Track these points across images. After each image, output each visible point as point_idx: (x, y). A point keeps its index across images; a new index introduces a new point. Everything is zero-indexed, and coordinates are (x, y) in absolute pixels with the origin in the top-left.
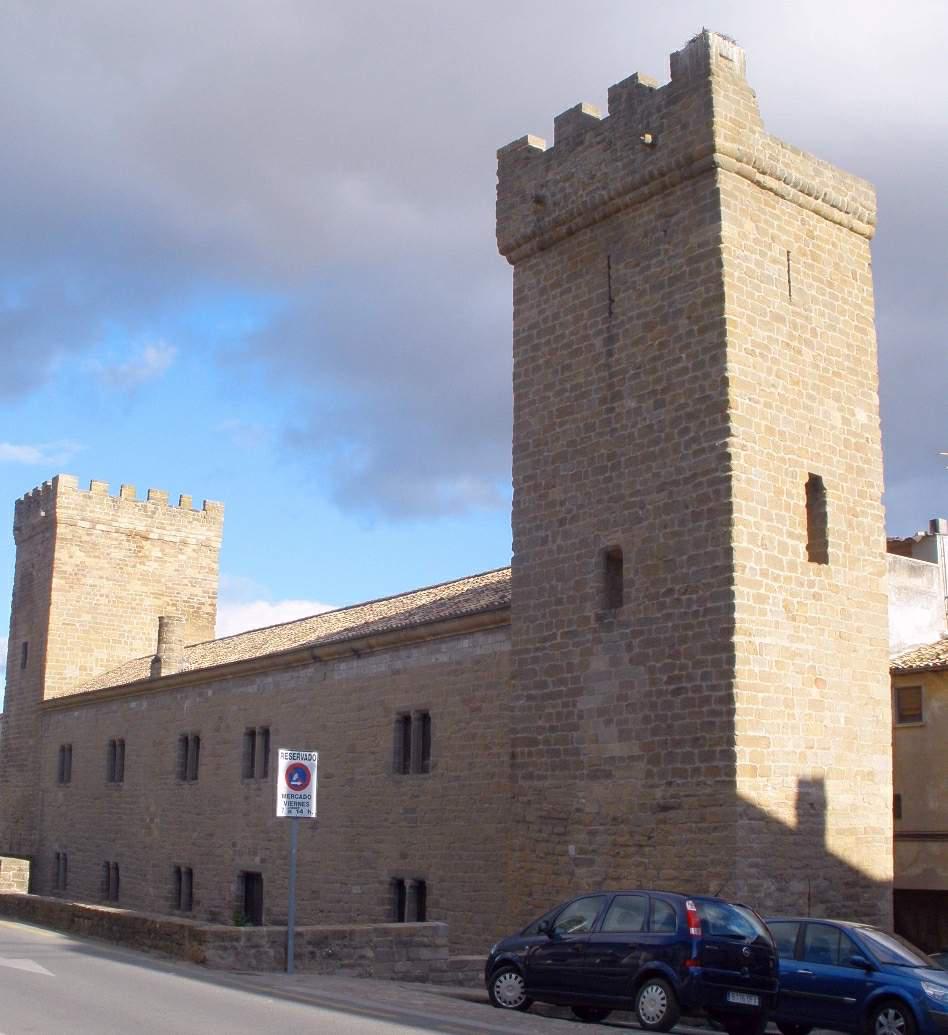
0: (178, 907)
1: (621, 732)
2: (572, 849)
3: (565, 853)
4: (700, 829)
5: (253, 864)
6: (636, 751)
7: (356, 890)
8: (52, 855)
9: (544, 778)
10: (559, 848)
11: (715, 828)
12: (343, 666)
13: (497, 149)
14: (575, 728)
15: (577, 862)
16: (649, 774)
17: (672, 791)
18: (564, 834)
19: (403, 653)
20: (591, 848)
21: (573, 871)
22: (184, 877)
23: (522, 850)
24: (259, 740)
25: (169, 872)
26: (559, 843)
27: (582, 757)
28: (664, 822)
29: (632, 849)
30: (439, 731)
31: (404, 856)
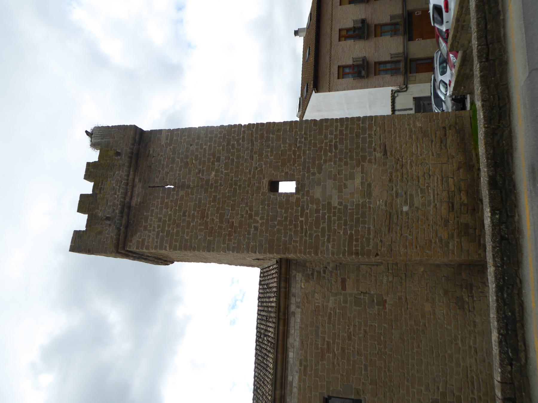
2: (405, 209)
3: (407, 213)
9: (369, 228)
21: (416, 207)
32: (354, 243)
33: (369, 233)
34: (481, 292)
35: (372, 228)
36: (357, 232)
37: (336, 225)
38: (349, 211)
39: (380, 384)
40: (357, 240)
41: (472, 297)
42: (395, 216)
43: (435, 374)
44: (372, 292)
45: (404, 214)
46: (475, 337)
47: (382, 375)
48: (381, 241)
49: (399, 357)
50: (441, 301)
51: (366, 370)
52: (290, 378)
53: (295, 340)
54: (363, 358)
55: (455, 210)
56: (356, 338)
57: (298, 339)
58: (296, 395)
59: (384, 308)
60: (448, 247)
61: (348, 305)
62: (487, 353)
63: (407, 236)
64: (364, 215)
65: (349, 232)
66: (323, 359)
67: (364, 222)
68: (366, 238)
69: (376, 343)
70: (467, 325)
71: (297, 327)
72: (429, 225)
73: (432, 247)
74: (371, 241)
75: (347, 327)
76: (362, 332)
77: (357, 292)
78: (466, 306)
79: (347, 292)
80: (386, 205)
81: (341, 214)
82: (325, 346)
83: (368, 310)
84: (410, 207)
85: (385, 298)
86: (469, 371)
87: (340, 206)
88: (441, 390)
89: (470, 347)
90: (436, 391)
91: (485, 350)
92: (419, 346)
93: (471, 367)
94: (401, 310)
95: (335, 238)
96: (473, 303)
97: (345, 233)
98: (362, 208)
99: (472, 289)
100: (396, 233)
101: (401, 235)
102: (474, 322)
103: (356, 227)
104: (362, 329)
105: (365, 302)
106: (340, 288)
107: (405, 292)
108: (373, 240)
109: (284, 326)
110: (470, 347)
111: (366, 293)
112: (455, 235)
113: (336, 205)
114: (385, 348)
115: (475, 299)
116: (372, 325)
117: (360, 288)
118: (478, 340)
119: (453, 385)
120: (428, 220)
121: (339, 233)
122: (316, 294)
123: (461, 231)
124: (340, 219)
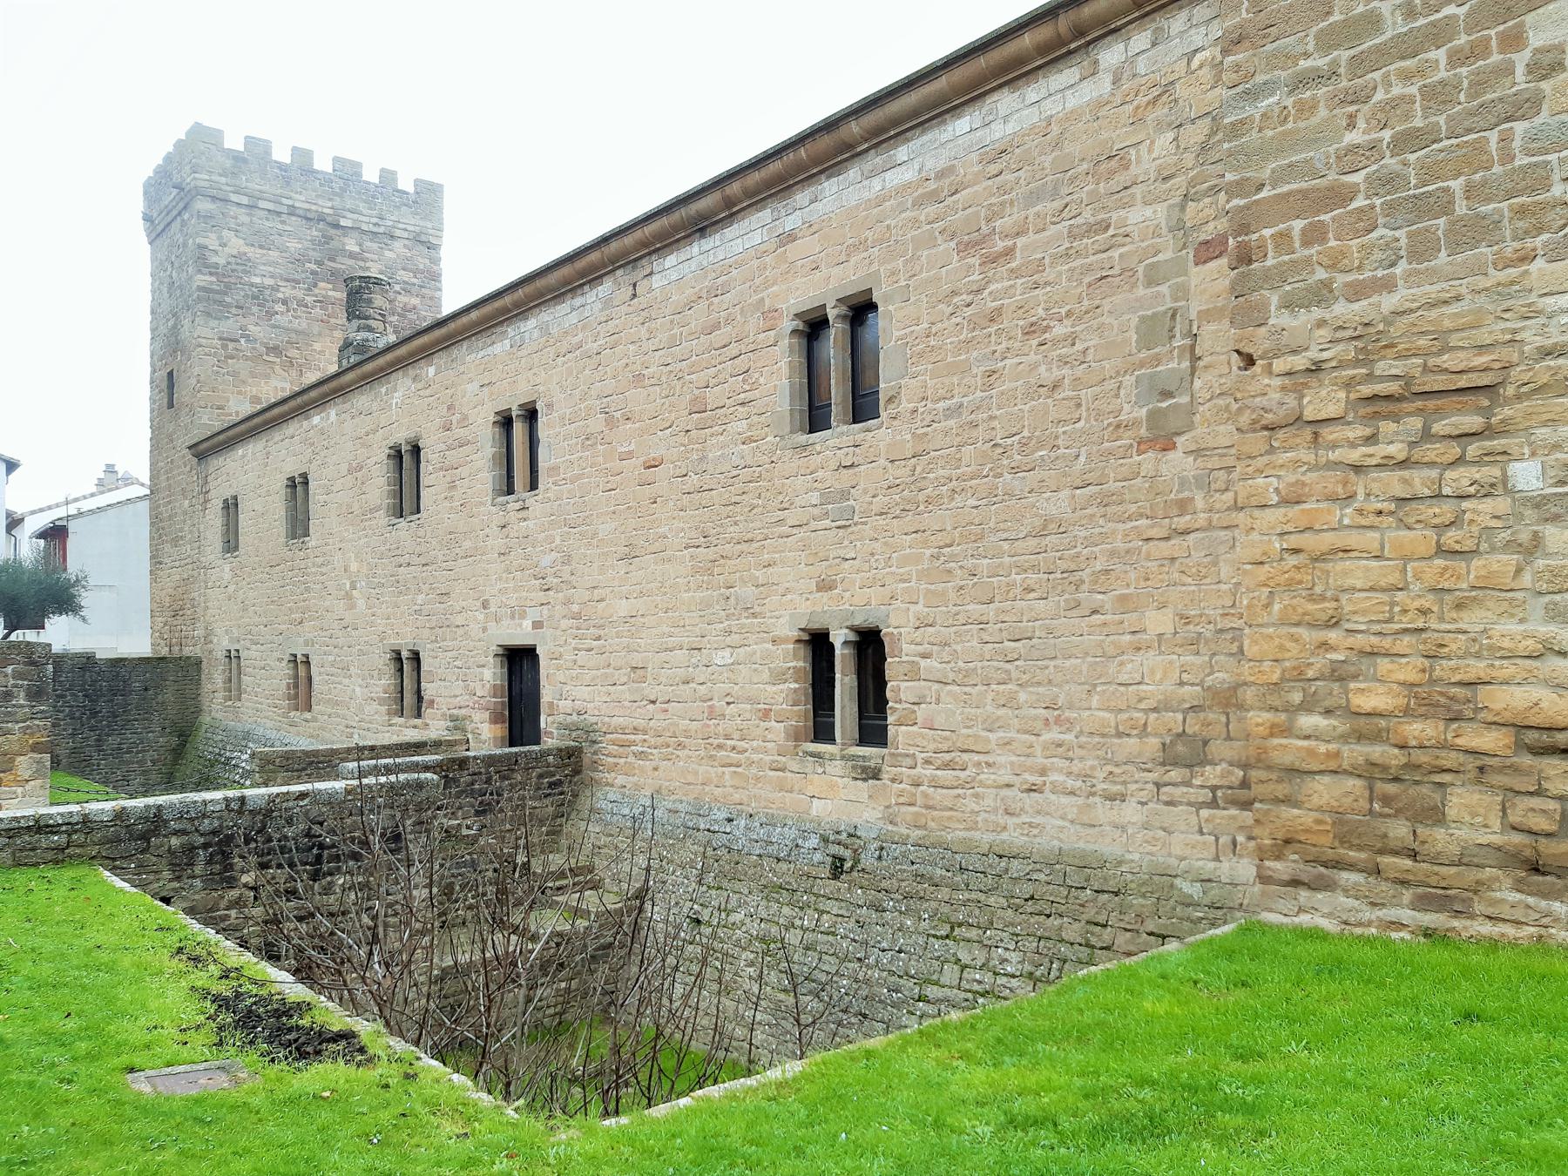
2: (1527, 475)
3: (1502, 486)
8: (220, 654)
9: (1388, 285)
12: (671, 260)
19: (801, 197)
21: (1537, 538)
22: (407, 664)
24: (519, 429)
25: (383, 661)
26: (1460, 461)
31: (825, 586)
32: (1298, 225)
33: (1356, 292)
34: (1234, 843)
35: (1389, 302)
36: (1366, 222)
37: (1396, 91)
38: (1493, 136)
39: (919, 469)
40: (1314, 235)
41: (1213, 804)
42: (1473, 422)
43: (958, 648)
44: (1198, 383)
45: (1490, 473)
46: (1072, 793)
47: (941, 472)
48: (1316, 369)
49: (992, 525)
50: (1185, 676)
51: (950, 413)
52: (902, 152)
53: (1006, 119)
54: (979, 394)
55: (1527, 760)
56: (1032, 357)
57: (1011, 128)
58: (866, 195)
59: (1142, 445)
60: (1306, 707)
61: (1141, 291)
62: (1030, 825)
63: (1351, 497)
64: (1475, 231)
65: (1357, 178)
66: (964, 248)
67: (1421, 249)
68: (1326, 285)
69: (1026, 433)
70: (1109, 768)
71: (1052, 107)
72: (1424, 612)
73: (1300, 630)
74: (1317, 313)
75: (1063, 311)
76: (1057, 373)
77: (1193, 315)
78: (1175, 774)
79: (1194, 270)
80: (1547, 353)
81: (1471, 97)
82: (1001, 245)
83: (1129, 380)
84: (1539, 503)
85: (1180, 440)
86: (976, 757)
87: (1531, 69)
88: (923, 663)
89: (1043, 772)
90: (919, 648)
91: (1038, 820)
92: (1029, 590)
93: (988, 765)
94: (1141, 515)
95: (1323, 112)
96: (1190, 804)
97: (1352, 158)
98: (1521, 212)
99: (1235, 803)
100: (1371, 439)
101: (1357, 468)
102: (1123, 798)
103: (1390, 208)
104: (1066, 371)
105: (1157, 360)
106: (1203, 237)
107: (1210, 527)
108: (1321, 323)
109: (1043, 49)
110: (1043, 772)
111: (1195, 359)
112: (1377, 752)
113: (1536, 40)
114: (1014, 470)
115: (1205, 813)
116: (1079, 405)
117: (1212, 327)
118: (1065, 800)
119: (938, 701)
120: (1459, 606)
121: (1352, 125)
122: (1170, 135)
123: (1396, 779)
124: (1437, 96)
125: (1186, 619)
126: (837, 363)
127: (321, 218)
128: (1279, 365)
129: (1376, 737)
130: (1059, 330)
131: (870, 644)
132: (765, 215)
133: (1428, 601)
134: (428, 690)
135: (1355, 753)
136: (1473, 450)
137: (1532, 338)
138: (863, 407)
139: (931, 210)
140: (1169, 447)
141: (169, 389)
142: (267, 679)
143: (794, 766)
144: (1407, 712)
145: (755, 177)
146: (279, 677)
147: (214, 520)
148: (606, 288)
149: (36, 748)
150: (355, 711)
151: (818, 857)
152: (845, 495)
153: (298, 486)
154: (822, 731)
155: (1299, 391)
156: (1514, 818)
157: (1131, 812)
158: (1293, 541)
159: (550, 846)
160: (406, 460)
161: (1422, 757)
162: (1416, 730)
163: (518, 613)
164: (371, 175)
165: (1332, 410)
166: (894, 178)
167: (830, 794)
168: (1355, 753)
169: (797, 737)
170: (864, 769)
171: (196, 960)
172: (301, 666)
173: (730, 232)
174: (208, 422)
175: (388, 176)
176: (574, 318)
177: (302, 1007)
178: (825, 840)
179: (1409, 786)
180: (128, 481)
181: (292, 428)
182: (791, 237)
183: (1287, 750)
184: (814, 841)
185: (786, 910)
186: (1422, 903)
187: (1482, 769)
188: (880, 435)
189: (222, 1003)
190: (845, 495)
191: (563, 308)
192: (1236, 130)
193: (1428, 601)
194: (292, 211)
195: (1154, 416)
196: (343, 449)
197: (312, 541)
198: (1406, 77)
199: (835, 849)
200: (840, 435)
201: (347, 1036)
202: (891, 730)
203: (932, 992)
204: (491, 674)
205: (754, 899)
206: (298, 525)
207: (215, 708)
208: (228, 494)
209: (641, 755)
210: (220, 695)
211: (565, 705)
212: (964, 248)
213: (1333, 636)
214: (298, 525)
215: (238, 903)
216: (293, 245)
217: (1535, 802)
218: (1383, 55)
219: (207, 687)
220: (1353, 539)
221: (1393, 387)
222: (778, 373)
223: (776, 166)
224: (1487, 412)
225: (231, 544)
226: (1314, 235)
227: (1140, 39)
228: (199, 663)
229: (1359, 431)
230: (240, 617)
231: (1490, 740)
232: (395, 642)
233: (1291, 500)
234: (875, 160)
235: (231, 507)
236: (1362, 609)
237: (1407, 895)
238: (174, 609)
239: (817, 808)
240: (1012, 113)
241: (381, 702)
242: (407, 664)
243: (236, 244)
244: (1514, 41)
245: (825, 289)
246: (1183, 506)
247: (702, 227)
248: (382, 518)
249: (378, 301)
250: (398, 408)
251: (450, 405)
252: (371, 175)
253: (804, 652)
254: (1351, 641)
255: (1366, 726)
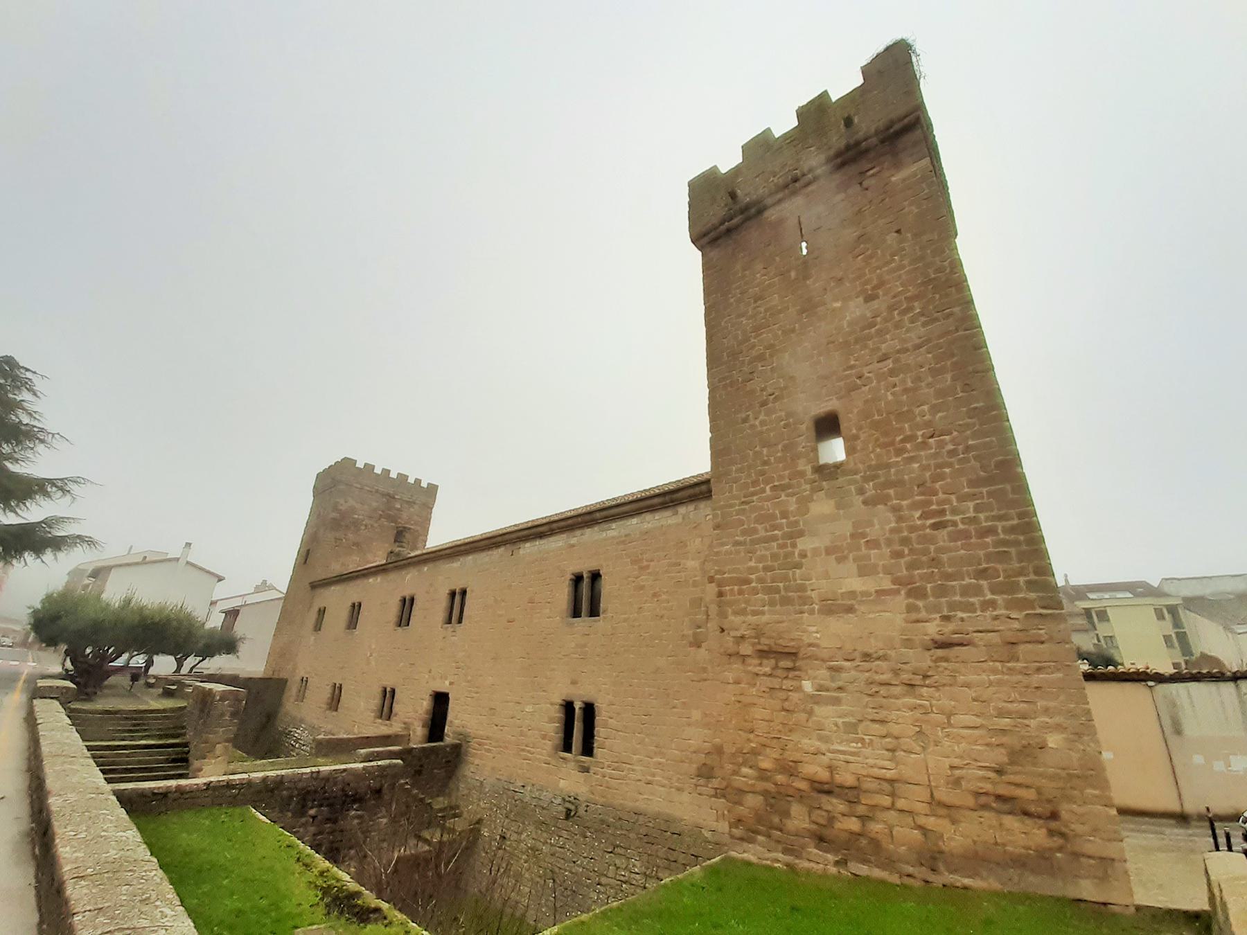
0: (381, 717)
1: (859, 568)
2: (807, 686)
3: (799, 689)
4: (1009, 669)
5: (443, 687)
6: (887, 584)
7: (529, 709)
8: (298, 678)
9: (763, 613)
10: (787, 684)
11: (1039, 670)
12: (528, 545)
13: (918, 47)
14: (798, 566)
15: (816, 700)
16: (911, 609)
17: (951, 627)
18: (793, 669)
19: (578, 533)
20: (834, 685)
21: (812, 709)
22: (388, 696)
23: (737, 682)
24: (458, 598)
25: (377, 692)
26: (786, 678)
27: (809, 593)
28: (946, 660)
29: (897, 690)
30: (607, 587)
31: (574, 683)
33: (755, 613)
36: (755, 592)
40: (741, 592)
41: (715, 796)
45: (794, 683)
48: (742, 637)
51: (625, 620)
52: (614, 525)
55: (815, 795)
59: (691, 645)
60: (744, 764)
64: (786, 601)
71: (663, 522)
78: (702, 781)
100: (760, 665)
124: (774, 557)
125: (706, 715)
126: (586, 595)
127: (388, 495)
128: (733, 633)
129: (766, 779)
130: (664, 597)
131: (589, 709)
132: (564, 536)
133: (780, 727)
134: (396, 707)
135: (762, 785)
136: (791, 674)
137: (807, 641)
138: (594, 612)
139: (622, 547)
140: (699, 647)
141: (306, 557)
142: (319, 694)
143: (553, 762)
144: (776, 770)
145: (563, 524)
146: (326, 693)
147: (313, 615)
148: (502, 550)
149: (227, 741)
150: (359, 718)
151: (560, 808)
152: (585, 646)
153: (356, 609)
154: (567, 747)
155: (738, 644)
156: (813, 818)
157: (685, 797)
158: (739, 698)
159: (441, 792)
160: (407, 604)
161: (782, 790)
162: (780, 778)
163: (443, 677)
164: (411, 480)
165: (749, 653)
166: (611, 533)
167: (568, 779)
168: (762, 785)
169: (556, 749)
170: (583, 767)
171: (306, 865)
172: (337, 692)
173: (551, 539)
174: (320, 574)
175: (418, 481)
176: (487, 559)
177: (358, 894)
178: (564, 799)
179: (777, 800)
180: (272, 588)
181: (359, 582)
182: (573, 546)
183: (739, 781)
184: (559, 801)
185: (545, 835)
186: (786, 851)
187: (801, 797)
188: (600, 623)
189: (326, 891)
190: (585, 646)
191: (483, 555)
192: (717, 554)
193: (780, 727)
194: (377, 491)
195: (695, 634)
196: (379, 596)
197: (357, 632)
198: (766, 549)
199: (568, 805)
200: (584, 622)
201: (377, 910)
202: (595, 751)
203: (604, 880)
204: (426, 704)
205: (531, 828)
206: (353, 623)
207: (290, 705)
208: (322, 606)
209: (488, 751)
210: (292, 700)
211: (457, 722)
212: (634, 562)
213: (751, 736)
214: (353, 623)
215: (303, 825)
216: (375, 504)
217: (819, 812)
218: (759, 541)
219: (287, 694)
220: (756, 700)
221: (766, 648)
222: (563, 595)
223: (570, 522)
224: (794, 661)
225: (318, 627)
226: (741, 592)
227: (691, 507)
228: (286, 681)
229: (757, 661)
230: (315, 664)
231: (803, 785)
232: (385, 683)
233: (737, 682)
234: (605, 526)
235: (322, 612)
236: (761, 727)
237: (780, 847)
238: (280, 653)
239: (562, 784)
240: (650, 521)
241: (373, 711)
242: (388, 696)
243: (351, 502)
244: (794, 545)
245: (584, 566)
246: (704, 670)
247: (541, 536)
248: (392, 626)
249: (407, 535)
250: (408, 582)
251: (430, 589)
252: (411, 480)
253: (563, 710)
254: (757, 739)
255: (763, 775)
